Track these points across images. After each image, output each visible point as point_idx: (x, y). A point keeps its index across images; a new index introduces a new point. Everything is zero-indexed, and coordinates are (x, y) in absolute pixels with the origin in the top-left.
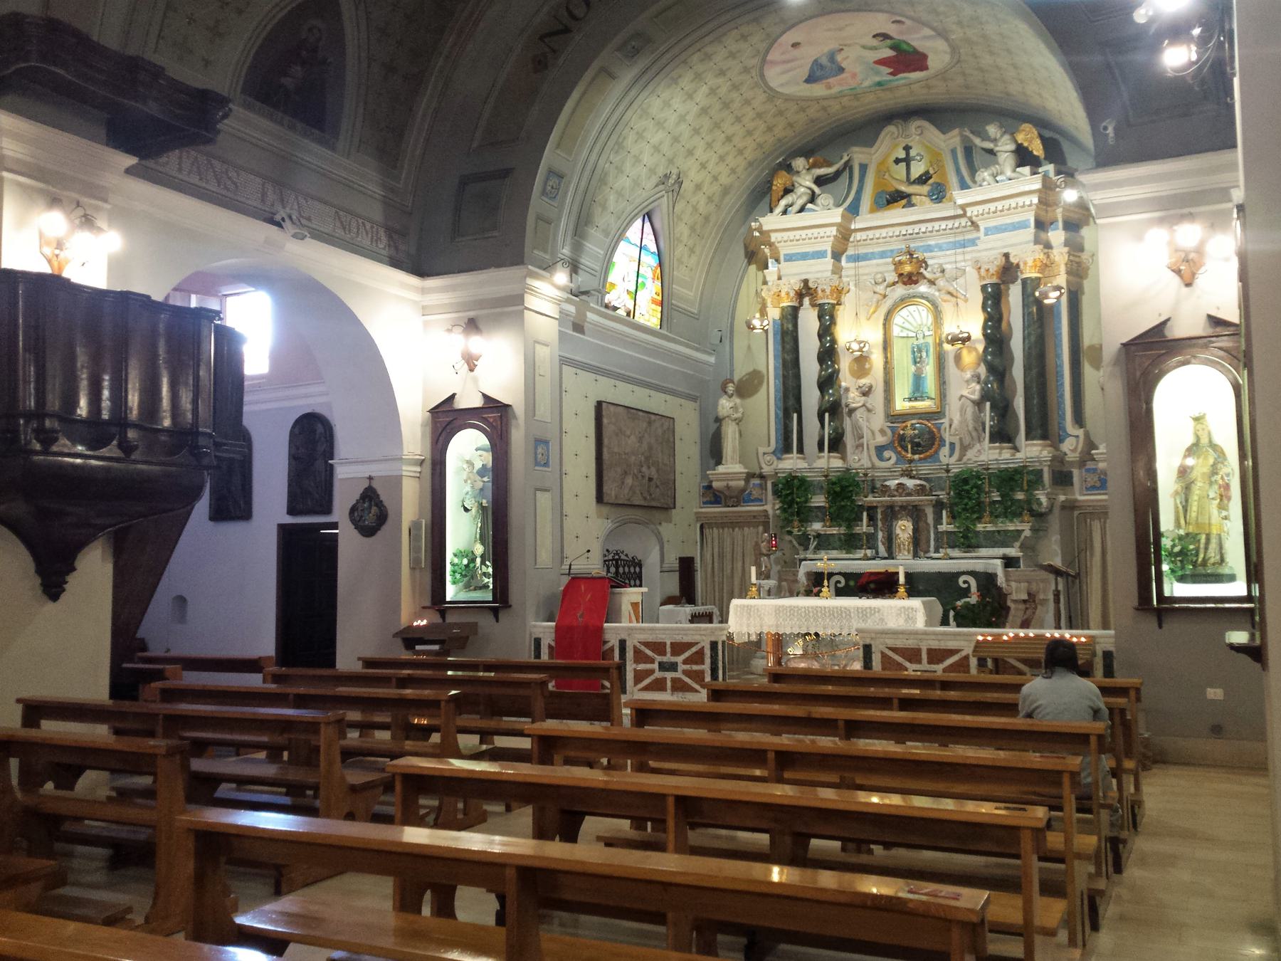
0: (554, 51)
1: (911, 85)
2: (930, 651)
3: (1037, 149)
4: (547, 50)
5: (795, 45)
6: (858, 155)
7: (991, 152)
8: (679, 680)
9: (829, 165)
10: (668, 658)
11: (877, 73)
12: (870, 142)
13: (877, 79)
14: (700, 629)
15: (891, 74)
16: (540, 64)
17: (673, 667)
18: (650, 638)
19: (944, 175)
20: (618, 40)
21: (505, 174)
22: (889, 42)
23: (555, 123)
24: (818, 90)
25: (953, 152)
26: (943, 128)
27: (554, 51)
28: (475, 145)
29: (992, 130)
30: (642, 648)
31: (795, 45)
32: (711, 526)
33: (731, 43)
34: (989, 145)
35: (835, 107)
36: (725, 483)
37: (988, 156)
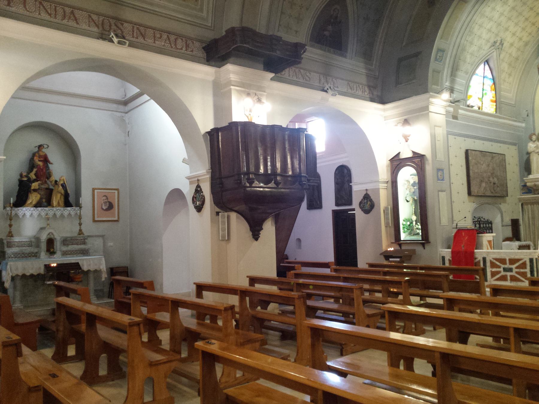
2: (510, 260)
8: (514, 276)
10: (507, 266)
14: (524, 253)
17: (510, 270)
18: (498, 257)
21: (417, 55)
28: (404, 44)
30: (494, 261)
32: (527, 204)
36: (533, 183)
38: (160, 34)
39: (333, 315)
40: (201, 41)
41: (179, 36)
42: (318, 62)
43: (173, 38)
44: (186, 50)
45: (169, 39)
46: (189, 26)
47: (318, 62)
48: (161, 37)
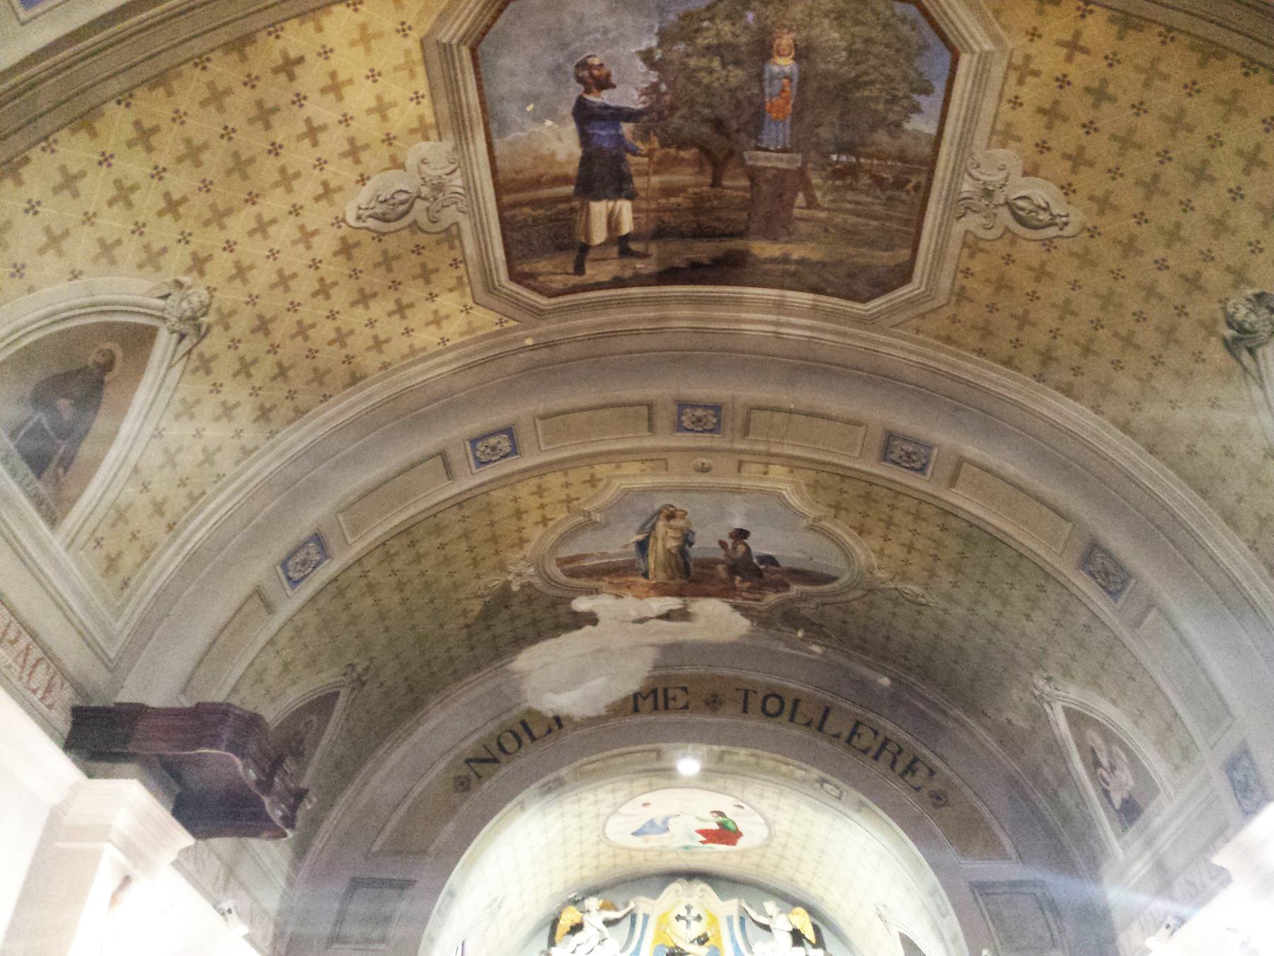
0: (479, 777)
1: (716, 856)
3: (809, 934)
4: (472, 774)
5: (645, 805)
6: (642, 904)
7: (767, 928)
9: (616, 909)
11: (691, 838)
12: (655, 894)
13: (689, 843)
15: (703, 842)
16: (463, 785)
19: (719, 939)
20: (542, 781)
22: (720, 819)
23: (469, 845)
24: (639, 842)
25: (730, 919)
26: (723, 895)
27: (479, 777)
28: (375, 848)
29: (770, 906)
31: (645, 805)
33: (601, 794)
34: (764, 921)
35: (639, 857)
37: (765, 933)
38: (19, 633)
39: (461, 26)
40: (78, 688)
41: (48, 655)
42: (72, 624)
43: (36, 653)
44: (42, 699)
45: (27, 655)
46: (75, 634)
47: (72, 624)
48: (16, 641)
